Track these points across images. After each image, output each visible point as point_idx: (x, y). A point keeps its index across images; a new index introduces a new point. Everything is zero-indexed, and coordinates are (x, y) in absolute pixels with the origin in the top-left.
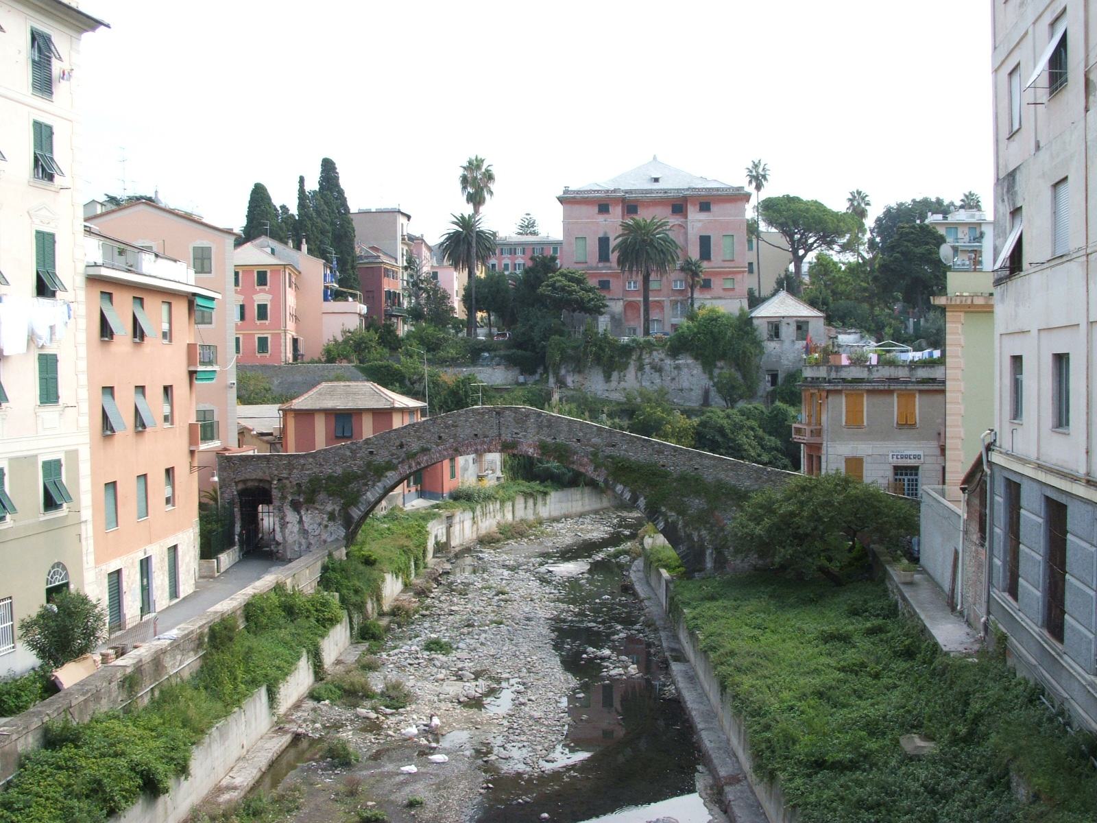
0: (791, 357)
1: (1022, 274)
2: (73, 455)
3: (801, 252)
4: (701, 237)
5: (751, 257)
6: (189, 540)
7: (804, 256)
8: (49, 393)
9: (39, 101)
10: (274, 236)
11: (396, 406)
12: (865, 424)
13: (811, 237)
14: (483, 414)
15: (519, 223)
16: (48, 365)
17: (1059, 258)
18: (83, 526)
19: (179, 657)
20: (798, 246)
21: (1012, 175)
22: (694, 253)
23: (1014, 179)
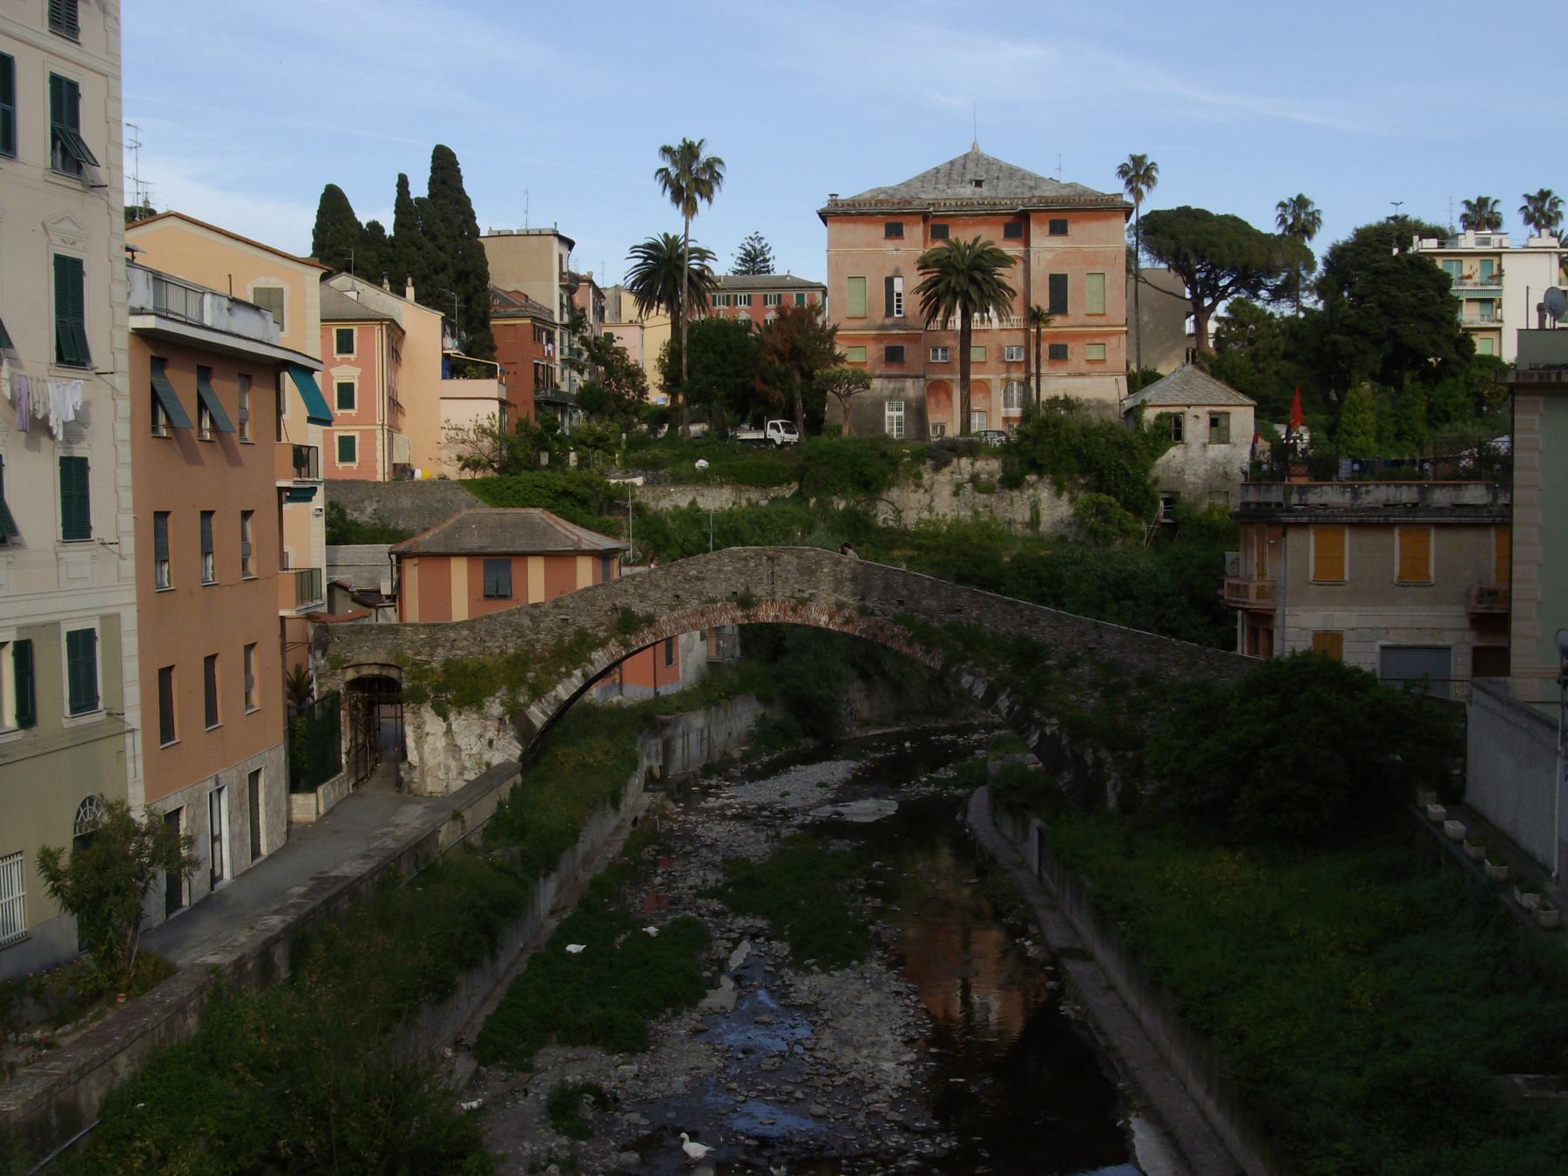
0: (1202, 470)
2: (111, 620)
3: (1207, 302)
7: (1212, 307)
8: (76, 523)
9: (60, 45)
12: (1347, 578)
13: (1223, 277)
15: (740, 253)
16: (74, 475)
18: (129, 738)
22: (1041, 299)
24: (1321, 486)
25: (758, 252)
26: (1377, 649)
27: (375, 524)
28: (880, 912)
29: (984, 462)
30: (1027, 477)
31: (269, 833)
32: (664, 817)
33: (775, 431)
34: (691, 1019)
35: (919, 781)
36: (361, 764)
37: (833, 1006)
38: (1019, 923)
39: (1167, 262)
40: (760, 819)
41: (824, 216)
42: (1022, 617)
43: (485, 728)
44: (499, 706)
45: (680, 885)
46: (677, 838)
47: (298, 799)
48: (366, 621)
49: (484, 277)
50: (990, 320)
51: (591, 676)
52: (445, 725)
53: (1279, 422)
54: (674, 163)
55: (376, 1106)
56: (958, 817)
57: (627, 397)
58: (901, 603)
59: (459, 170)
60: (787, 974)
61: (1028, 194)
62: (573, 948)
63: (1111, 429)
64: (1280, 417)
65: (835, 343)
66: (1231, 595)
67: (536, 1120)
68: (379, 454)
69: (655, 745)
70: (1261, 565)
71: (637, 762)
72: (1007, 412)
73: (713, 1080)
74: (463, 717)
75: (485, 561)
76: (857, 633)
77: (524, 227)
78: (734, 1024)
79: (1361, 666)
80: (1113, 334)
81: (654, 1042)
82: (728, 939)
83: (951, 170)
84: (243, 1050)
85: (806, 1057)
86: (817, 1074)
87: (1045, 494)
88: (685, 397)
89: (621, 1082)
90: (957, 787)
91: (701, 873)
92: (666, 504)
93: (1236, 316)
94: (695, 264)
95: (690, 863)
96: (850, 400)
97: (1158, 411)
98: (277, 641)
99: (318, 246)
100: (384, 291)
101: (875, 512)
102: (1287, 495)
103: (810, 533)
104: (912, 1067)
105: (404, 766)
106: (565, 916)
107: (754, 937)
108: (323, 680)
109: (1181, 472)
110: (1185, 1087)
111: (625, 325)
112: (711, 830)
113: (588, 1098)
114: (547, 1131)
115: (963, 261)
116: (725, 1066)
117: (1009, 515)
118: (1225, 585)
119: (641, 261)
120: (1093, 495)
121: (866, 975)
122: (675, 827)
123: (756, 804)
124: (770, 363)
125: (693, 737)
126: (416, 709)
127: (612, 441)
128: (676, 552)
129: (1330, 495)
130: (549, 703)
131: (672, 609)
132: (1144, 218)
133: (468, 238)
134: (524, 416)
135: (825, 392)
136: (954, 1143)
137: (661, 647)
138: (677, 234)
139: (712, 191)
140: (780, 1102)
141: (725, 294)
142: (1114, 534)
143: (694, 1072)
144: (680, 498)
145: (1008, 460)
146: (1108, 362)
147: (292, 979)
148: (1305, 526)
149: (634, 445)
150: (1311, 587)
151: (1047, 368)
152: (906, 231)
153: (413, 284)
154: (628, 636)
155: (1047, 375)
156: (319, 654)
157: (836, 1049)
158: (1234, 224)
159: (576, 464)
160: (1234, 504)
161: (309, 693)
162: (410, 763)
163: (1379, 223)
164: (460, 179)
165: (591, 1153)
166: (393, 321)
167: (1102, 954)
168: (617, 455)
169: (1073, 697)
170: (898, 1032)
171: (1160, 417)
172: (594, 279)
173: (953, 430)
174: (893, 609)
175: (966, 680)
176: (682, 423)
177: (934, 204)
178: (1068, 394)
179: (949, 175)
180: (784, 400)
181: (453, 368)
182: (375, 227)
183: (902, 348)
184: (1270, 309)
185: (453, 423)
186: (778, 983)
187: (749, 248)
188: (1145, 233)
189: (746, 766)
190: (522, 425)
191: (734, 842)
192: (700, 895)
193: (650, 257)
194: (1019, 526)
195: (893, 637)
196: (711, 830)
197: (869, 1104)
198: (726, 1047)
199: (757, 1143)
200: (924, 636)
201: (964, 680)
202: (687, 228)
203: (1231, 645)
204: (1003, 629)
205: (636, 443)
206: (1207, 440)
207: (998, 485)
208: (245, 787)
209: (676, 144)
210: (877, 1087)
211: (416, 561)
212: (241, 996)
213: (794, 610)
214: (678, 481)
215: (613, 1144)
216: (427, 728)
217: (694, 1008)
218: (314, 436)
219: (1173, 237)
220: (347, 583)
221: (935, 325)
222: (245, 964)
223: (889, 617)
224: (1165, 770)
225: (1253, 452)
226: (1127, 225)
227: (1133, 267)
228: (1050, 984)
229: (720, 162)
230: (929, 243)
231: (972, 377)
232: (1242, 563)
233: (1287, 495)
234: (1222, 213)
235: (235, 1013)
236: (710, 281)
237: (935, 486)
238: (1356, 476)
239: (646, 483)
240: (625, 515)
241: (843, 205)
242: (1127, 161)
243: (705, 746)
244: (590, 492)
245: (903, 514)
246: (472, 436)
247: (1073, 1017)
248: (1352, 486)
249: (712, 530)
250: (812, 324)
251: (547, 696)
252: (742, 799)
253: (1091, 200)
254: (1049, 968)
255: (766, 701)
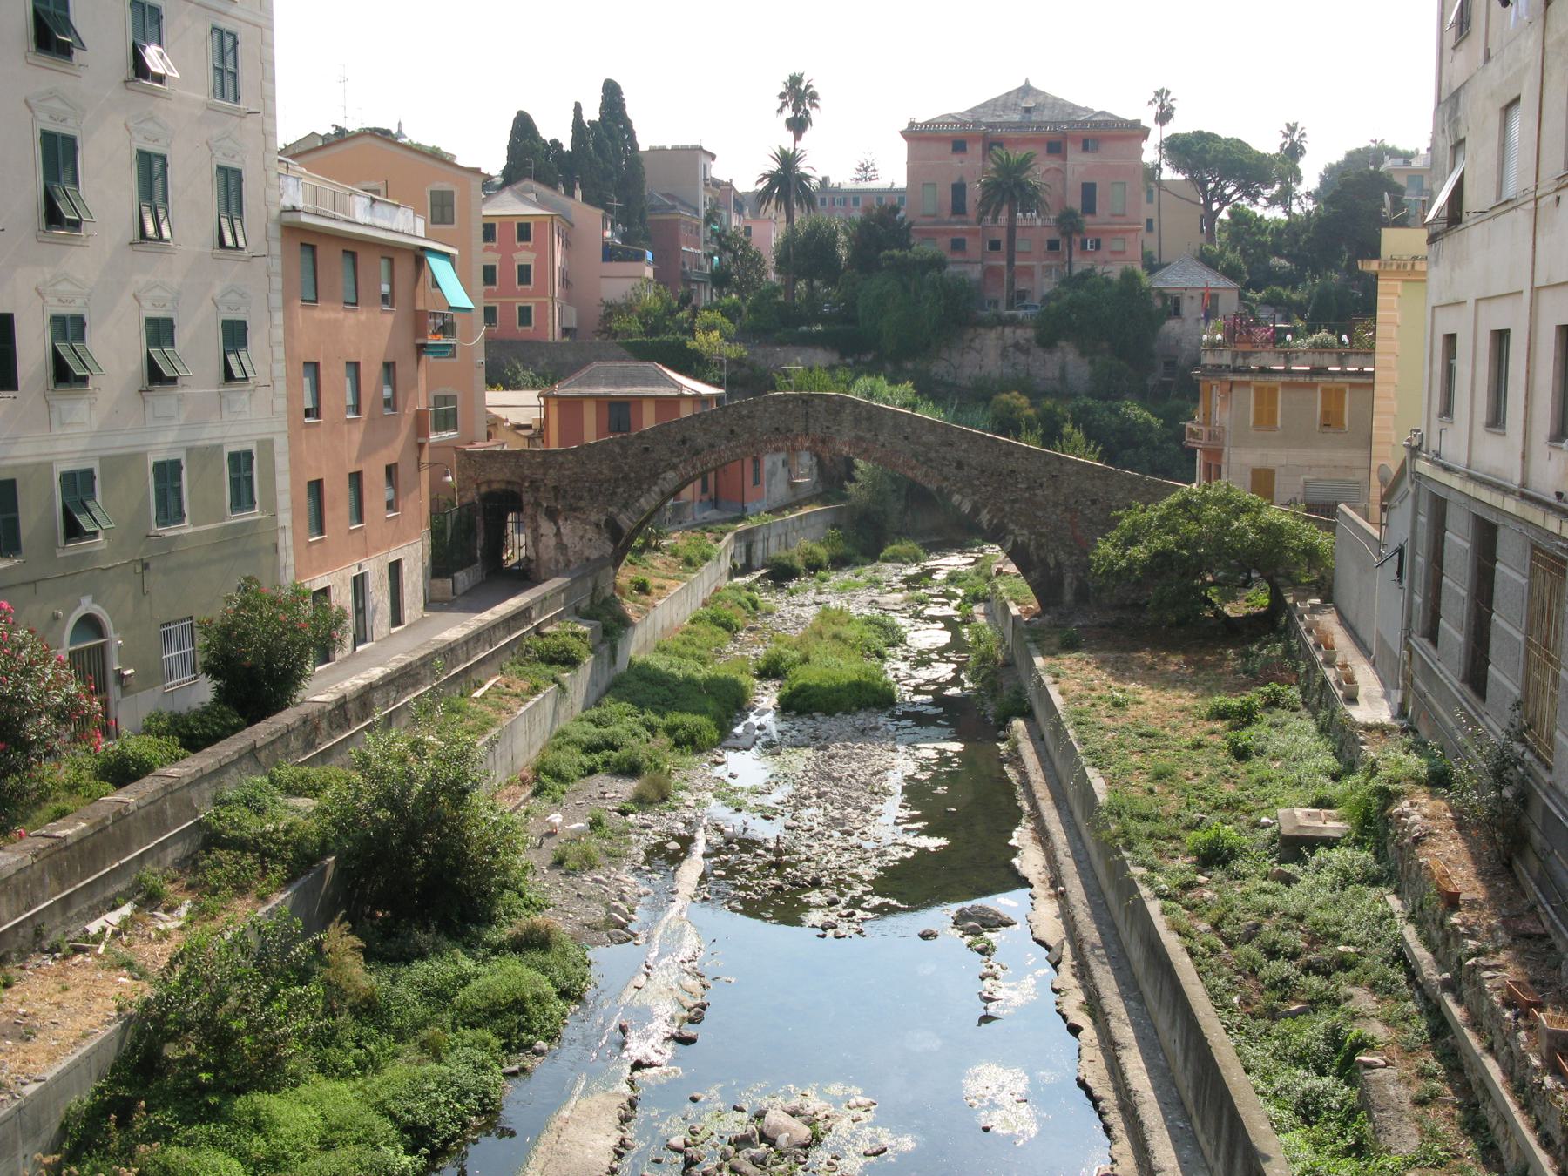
1: (1461, 227)
2: (267, 445)
3: (1215, 206)
4: (1084, 185)
5: (1148, 211)
6: (414, 555)
10: (538, 178)
11: (686, 392)
12: (1279, 424)
14: (786, 402)
17: (1505, 204)
19: (393, 694)
20: (1212, 197)
21: (1455, 96)
22: (1075, 202)
23: (1457, 102)
131: (729, 440)
152: (968, 147)
175: (956, 498)
182: (556, 144)
183: (964, 240)
234: (1229, 136)
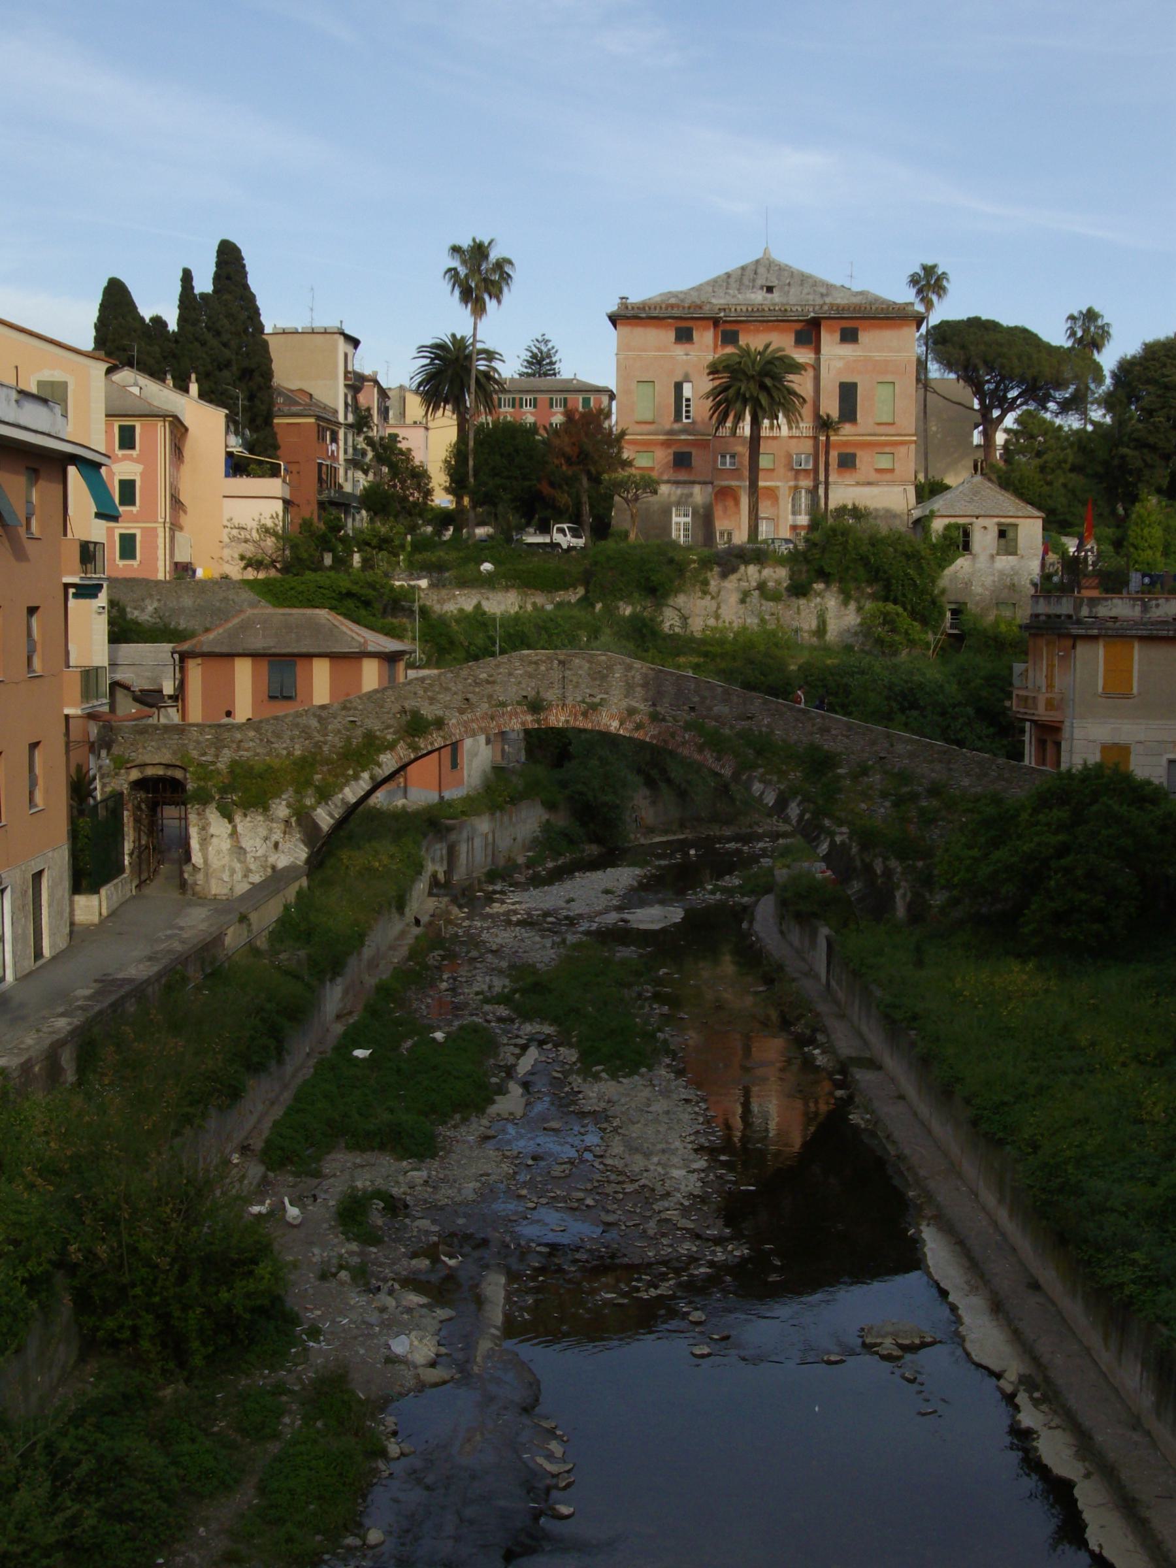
0: (989, 581)
3: (996, 413)
7: (1001, 419)
12: (1135, 691)
13: (1012, 388)
15: (526, 355)
22: (831, 407)
24: (1112, 599)
25: (545, 355)
26: (1164, 762)
27: (155, 623)
28: (667, 1019)
29: (772, 570)
30: (815, 586)
31: (52, 935)
32: (449, 922)
33: (561, 535)
34: (477, 1126)
35: (705, 889)
36: (144, 867)
37: (622, 1113)
38: (808, 1032)
39: (956, 373)
40: (546, 925)
41: (614, 319)
42: (813, 725)
43: (271, 830)
44: (284, 808)
45: (466, 990)
46: (463, 942)
47: (81, 900)
48: (150, 721)
49: (268, 374)
50: (779, 427)
51: (379, 779)
52: (230, 826)
53: (1067, 535)
54: (464, 262)
55: (168, 1211)
56: (745, 925)
57: (411, 499)
58: (692, 709)
59: (244, 266)
60: (576, 1080)
61: (819, 301)
62: (360, 1053)
63: (899, 539)
64: (1069, 530)
65: (623, 448)
66: (1018, 706)
67: (325, 1226)
68: (161, 552)
69: (440, 849)
70: (1050, 677)
71: (422, 866)
72: (794, 520)
73: (502, 1186)
74: (248, 819)
75: (269, 661)
76: (648, 739)
77: (309, 325)
78: (523, 1131)
79: (1152, 779)
80: (902, 443)
81: (443, 1149)
82: (516, 1045)
83: (742, 275)
84: (30, 1154)
85: (596, 1164)
86: (608, 1181)
87: (832, 602)
88: (471, 500)
89: (410, 1188)
90: (743, 895)
91: (487, 979)
92: (451, 608)
93: (1025, 428)
94: (482, 365)
95: (475, 968)
96: (638, 505)
97: (947, 521)
98: (62, 740)
99: (100, 342)
100: (168, 387)
101: (661, 618)
102: (1078, 607)
103: (596, 638)
104: (703, 1175)
105: (187, 869)
106: (351, 1021)
107: (541, 1043)
108: (106, 780)
109: (968, 584)
110: (976, 1195)
111: (409, 426)
112: (497, 936)
113: (377, 1204)
114: (337, 1236)
115: (753, 367)
116: (515, 1173)
117: (795, 624)
118: (1014, 696)
119: (427, 361)
120: (880, 604)
121: (654, 1082)
122: (460, 932)
123: (541, 909)
124: (557, 467)
125: (478, 842)
126: (200, 810)
127: (397, 542)
128: (461, 655)
129: (1120, 608)
130: (336, 806)
131: (462, 712)
132: (934, 327)
133: (253, 335)
134: (307, 516)
135: (612, 497)
136: (746, 1251)
137: (447, 753)
138: (464, 335)
139: (501, 291)
140: (571, 1209)
141: (511, 396)
142: (901, 644)
143: (483, 1179)
144: (464, 602)
145: (795, 569)
146: (897, 472)
147: (80, 1083)
148: (1095, 638)
149: (420, 546)
150: (1100, 699)
151: (836, 476)
152: (695, 335)
153: (197, 380)
154: (417, 739)
155: (835, 483)
156: (104, 753)
157: (627, 1156)
158: (1024, 336)
159: (360, 565)
160: (1023, 615)
161: (90, 793)
162: (193, 865)
163: (1167, 338)
164: (244, 275)
165: (382, 1259)
166: (176, 417)
167: (890, 1062)
168: (401, 557)
169: (864, 806)
170: (689, 1139)
171: (948, 527)
172: (379, 379)
173: (741, 537)
174: (685, 716)
175: (757, 787)
176: (467, 526)
177: (724, 310)
178: (857, 504)
179: (740, 280)
180: (570, 503)
181: (236, 467)
182: (158, 322)
183: (690, 454)
184: (1058, 421)
185: (236, 522)
186: (566, 1089)
187: (535, 350)
188: (935, 343)
189: (531, 872)
190: (306, 525)
191: (519, 947)
192: (487, 1001)
193: (437, 357)
194: (806, 635)
195: (684, 743)
196: (497, 936)
197: (660, 1212)
198: (515, 1153)
199: (548, 1250)
200: (715, 743)
201: (755, 788)
202: (475, 329)
203: (1020, 756)
204: (795, 737)
205: (420, 546)
206: (995, 552)
207: (785, 593)
208: (28, 887)
209: (466, 243)
210: (668, 1194)
211: (199, 661)
212: (28, 1099)
213: (585, 714)
214: (464, 583)
215: (403, 1250)
216: (212, 830)
217: (483, 1114)
218: (98, 531)
219: (963, 347)
220: (128, 682)
221: (724, 431)
222: (32, 1066)
223: (680, 723)
224: (956, 880)
225: (1043, 565)
226: (918, 334)
227: (923, 377)
228: (839, 1093)
229: (510, 262)
230: (719, 348)
231: (761, 484)
232: (1030, 674)
233: (1078, 607)
234: (1012, 324)
235: (22, 1117)
236: (496, 382)
237: (722, 593)
238: (1149, 589)
239: (432, 586)
240: (408, 617)
241: (633, 308)
242: (918, 270)
243: (490, 852)
244: (374, 593)
245: (690, 621)
246: (255, 535)
247: (863, 1126)
248: (1142, 599)
249: (498, 634)
250: (600, 426)
251: (333, 798)
252: (527, 905)
253: (882, 309)
254: (838, 1077)
255: (551, 806)
